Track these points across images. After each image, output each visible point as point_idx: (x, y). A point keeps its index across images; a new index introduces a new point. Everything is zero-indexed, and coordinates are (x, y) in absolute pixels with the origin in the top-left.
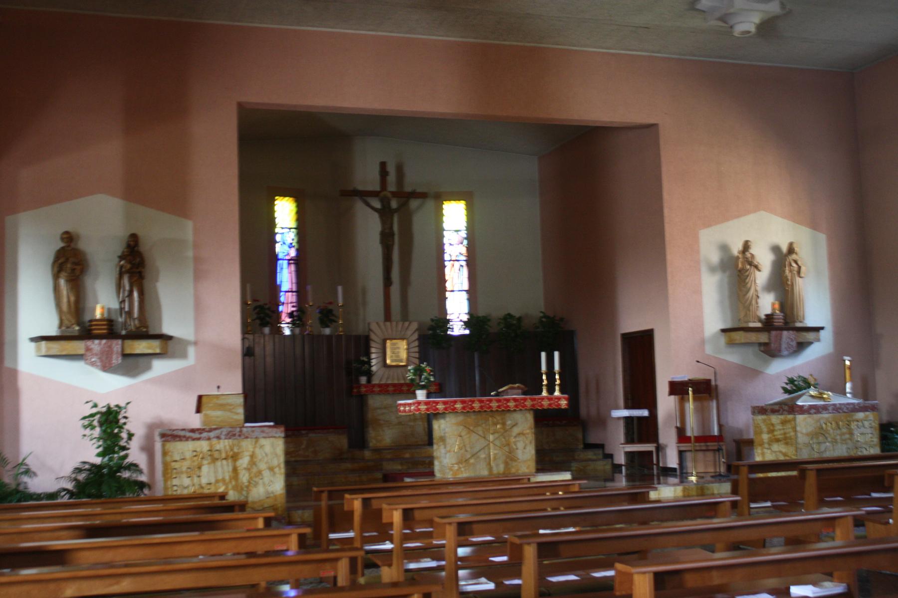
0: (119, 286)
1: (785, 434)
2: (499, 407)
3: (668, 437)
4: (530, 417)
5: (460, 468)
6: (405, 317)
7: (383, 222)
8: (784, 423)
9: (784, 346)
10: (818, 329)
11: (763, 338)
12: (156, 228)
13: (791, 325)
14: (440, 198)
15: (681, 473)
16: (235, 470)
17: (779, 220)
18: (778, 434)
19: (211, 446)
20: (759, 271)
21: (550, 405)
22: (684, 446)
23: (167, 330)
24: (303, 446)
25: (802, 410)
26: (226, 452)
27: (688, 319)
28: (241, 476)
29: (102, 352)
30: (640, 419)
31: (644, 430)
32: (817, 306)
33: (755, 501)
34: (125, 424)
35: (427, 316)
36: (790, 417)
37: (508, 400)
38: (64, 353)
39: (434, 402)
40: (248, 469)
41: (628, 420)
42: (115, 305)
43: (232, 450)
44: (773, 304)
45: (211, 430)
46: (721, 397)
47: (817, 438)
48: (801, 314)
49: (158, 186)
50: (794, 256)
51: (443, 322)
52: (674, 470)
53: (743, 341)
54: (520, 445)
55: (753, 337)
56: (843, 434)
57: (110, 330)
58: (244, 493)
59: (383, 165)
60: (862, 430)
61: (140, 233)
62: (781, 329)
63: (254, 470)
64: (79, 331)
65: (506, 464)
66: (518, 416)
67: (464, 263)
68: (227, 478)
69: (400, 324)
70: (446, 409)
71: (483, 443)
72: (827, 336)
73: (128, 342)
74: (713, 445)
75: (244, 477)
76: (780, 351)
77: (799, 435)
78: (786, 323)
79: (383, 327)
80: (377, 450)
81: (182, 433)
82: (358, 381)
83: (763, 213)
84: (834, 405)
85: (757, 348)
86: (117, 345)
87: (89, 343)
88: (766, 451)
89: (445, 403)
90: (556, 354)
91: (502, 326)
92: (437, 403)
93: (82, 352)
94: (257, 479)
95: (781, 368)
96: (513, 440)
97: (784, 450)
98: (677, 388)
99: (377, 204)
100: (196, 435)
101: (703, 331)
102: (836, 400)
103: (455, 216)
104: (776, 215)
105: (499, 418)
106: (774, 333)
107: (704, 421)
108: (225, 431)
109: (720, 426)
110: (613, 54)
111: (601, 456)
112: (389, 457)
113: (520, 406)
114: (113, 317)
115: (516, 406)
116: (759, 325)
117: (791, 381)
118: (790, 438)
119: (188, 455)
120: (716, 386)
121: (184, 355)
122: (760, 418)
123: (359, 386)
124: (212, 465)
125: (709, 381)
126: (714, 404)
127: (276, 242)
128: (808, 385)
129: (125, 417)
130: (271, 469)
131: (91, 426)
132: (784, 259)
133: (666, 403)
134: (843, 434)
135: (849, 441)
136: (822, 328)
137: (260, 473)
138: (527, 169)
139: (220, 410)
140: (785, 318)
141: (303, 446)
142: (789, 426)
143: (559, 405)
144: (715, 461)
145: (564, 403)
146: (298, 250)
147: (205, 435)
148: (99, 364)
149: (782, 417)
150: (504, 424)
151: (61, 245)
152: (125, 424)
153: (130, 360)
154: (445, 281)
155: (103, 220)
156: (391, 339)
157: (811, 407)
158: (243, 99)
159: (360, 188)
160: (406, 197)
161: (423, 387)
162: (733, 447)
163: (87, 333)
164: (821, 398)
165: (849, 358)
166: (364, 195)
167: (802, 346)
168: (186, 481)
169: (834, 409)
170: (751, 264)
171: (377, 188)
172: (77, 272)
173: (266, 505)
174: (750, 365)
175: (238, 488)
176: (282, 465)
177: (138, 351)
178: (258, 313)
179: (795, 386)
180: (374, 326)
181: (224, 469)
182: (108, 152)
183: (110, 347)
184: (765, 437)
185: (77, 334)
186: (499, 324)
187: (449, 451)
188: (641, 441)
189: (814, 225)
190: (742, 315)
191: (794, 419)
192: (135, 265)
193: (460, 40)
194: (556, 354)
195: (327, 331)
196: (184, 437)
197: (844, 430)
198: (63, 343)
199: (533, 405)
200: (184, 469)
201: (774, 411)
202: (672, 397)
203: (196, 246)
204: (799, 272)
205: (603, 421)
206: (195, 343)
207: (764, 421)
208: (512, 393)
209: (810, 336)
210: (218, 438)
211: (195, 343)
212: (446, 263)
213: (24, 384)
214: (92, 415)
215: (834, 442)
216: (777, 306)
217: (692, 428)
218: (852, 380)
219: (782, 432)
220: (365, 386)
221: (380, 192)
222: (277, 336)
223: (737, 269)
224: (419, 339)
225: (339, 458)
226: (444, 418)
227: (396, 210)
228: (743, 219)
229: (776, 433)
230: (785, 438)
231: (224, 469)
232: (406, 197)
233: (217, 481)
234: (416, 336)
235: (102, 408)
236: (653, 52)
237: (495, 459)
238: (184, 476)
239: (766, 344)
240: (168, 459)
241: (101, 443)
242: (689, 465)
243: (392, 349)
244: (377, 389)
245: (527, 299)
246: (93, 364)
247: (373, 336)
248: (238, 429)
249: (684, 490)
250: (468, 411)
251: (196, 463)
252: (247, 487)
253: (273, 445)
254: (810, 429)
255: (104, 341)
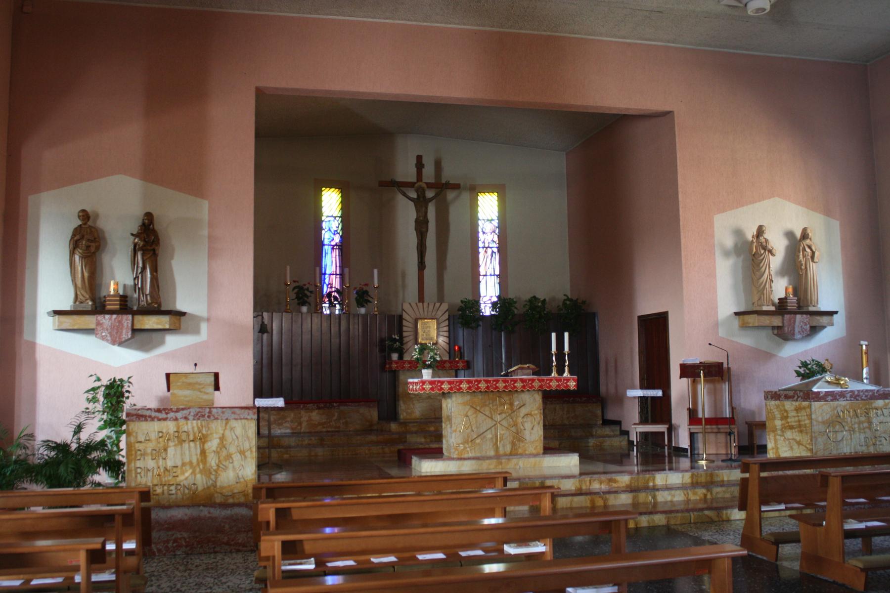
0: (134, 262)
1: (799, 421)
2: (505, 387)
3: (679, 417)
4: (538, 398)
5: (465, 448)
6: (441, 299)
7: (418, 211)
8: (798, 410)
9: (797, 330)
10: (831, 314)
11: (777, 321)
12: (172, 208)
13: (805, 309)
14: (475, 190)
15: (692, 453)
16: (203, 452)
17: (793, 206)
18: (792, 421)
19: (178, 427)
20: (773, 255)
21: (558, 386)
22: (696, 428)
23: (180, 306)
24: (335, 418)
25: (818, 397)
26: (194, 434)
27: (701, 301)
28: (209, 459)
29: (112, 327)
30: (654, 399)
31: (657, 410)
32: (830, 290)
33: (767, 503)
34: (128, 398)
35: (456, 296)
36: (805, 404)
37: (515, 381)
38: (75, 327)
39: (439, 381)
40: (217, 452)
41: (643, 400)
42: (130, 282)
43: (200, 432)
44: (786, 289)
45: (178, 410)
46: (733, 379)
47: (834, 427)
48: (814, 298)
49: (176, 167)
50: (808, 242)
51: (475, 303)
52: (685, 450)
53: (757, 324)
54: (528, 426)
55: (766, 320)
56: (862, 422)
57: (125, 306)
58: (213, 477)
59: (419, 158)
60: (881, 418)
61: (156, 214)
62: (795, 313)
63: (224, 453)
64: (91, 304)
65: (513, 444)
66: (526, 397)
67: (495, 250)
68: (195, 461)
69: (438, 305)
70: (451, 389)
71: (490, 423)
72: (839, 320)
73: (138, 318)
74: (724, 428)
75: (212, 461)
76: (794, 334)
77: (815, 423)
78: (799, 307)
79: (415, 308)
80: (404, 424)
81: (148, 413)
82: (390, 357)
83: (777, 199)
84: (852, 391)
85: (770, 332)
86: (127, 320)
87: (100, 318)
88: (778, 437)
89: (450, 383)
90: (566, 335)
91: (527, 307)
92: (442, 383)
93: (93, 326)
94: (227, 463)
95: (795, 352)
96: (520, 420)
97: (798, 439)
98: (687, 371)
99: (414, 195)
100: (163, 415)
101: (716, 313)
102: (854, 386)
103: (488, 206)
104: (789, 200)
105: (507, 398)
106: (787, 317)
107: (716, 404)
108: (193, 411)
109: (733, 409)
110: (630, 44)
111: (618, 433)
112: (414, 429)
113: (527, 386)
114: (129, 292)
115: (524, 387)
116: (773, 308)
117: (804, 364)
118: (805, 426)
119: (153, 436)
120: (729, 369)
121: (196, 331)
122: (773, 403)
123: (391, 362)
124: (179, 448)
125: (722, 363)
126: (726, 386)
127: (322, 229)
128: (822, 370)
129: (128, 391)
130: (242, 453)
131: (94, 400)
132: (798, 244)
133: (679, 386)
134: (862, 422)
135: (867, 430)
136: (836, 312)
137: (229, 457)
138: (555, 163)
139: (188, 389)
140: (799, 301)
141: (335, 418)
142: (803, 413)
143: (568, 386)
144: (727, 443)
145: (572, 385)
146: (341, 237)
147: (172, 415)
148: (109, 338)
149: (797, 403)
150: (511, 404)
151: (80, 223)
152: (128, 398)
153: (139, 336)
154: (479, 266)
155: (120, 201)
156: (421, 319)
157: (827, 394)
158: (260, 84)
159: (399, 179)
160: (442, 187)
161: (428, 367)
162: (745, 429)
163: (99, 308)
164: (837, 383)
165: (866, 343)
166: (402, 186)
167: (814, 330)
168: (151, 464)
169: (851, 396)
170: (765, 248)
171: (413, 179)
172: (93, 249)
173: (236, 491)
174: (763, 348)
175: (207, 472)
176: (254, 449)
177: (147, 327)
178: (297, 293)
179: (809, 369)
180: (406, 306)
181: (191, 452)
182: (129, 134)
183: (120, 322)
184: (778, 423)
185: (89, 309)
186: (524, 306)
187: (455, 431)
188: (655, 422)
189: (827, 212)
190: (756, 298)
191: (810, 407)
192: (149, 242)
193: (475, 28)
194: (566, 335)
195: (363, 311)
196: (150, 417)
197: (863, 419)
198: (75, 317)
199: (541, 386)
200: (149, 451)
201: (787, 397)
202: (685, 380)
203: (211, 225)
204: (813, 257)
205: (620, 399)
206: (208, 320)
207: (777, 406)
208: (522, 374)
209: (824, 320)
210: (186, 418)
211: (208, 320)
212: (481, 250)
213: (40, 355)
214: (93, 389)
215: (852, 430)
216: (791, 290)
217: (705, 411)
218: (868, 365)
219: (797, 419)
220: (396, 362)
221: (415, 183)
222: (315, 315)
223: (751, 253)
224: (449, 319)
225: (369, 429)
226: (450, 397)
227: (431, 200)
228: (757, 205)
229: (789, 420)
230: (800, 426)
231: (191, 452)
232: (442, 187)
233: (184, 464)
234: (446, 316)
235: (105, 381)
236: (669, 42)
237: (502, 439)
238: (149, 458)
239: (779, 328)
240: (132, 439)
241: (105, 417)
242: (700, 445)
243: (423, 328)
244: (407, 365)
245: (553, 283)
246: (103, 338)
247: (405, 316)
248: (208, 410)
249: (692, 476)
250: (474, 390)
251: (162, 445)
252: (216, 471)
253: (244, 427)
254: (827, 417)
255: (114, 316)
